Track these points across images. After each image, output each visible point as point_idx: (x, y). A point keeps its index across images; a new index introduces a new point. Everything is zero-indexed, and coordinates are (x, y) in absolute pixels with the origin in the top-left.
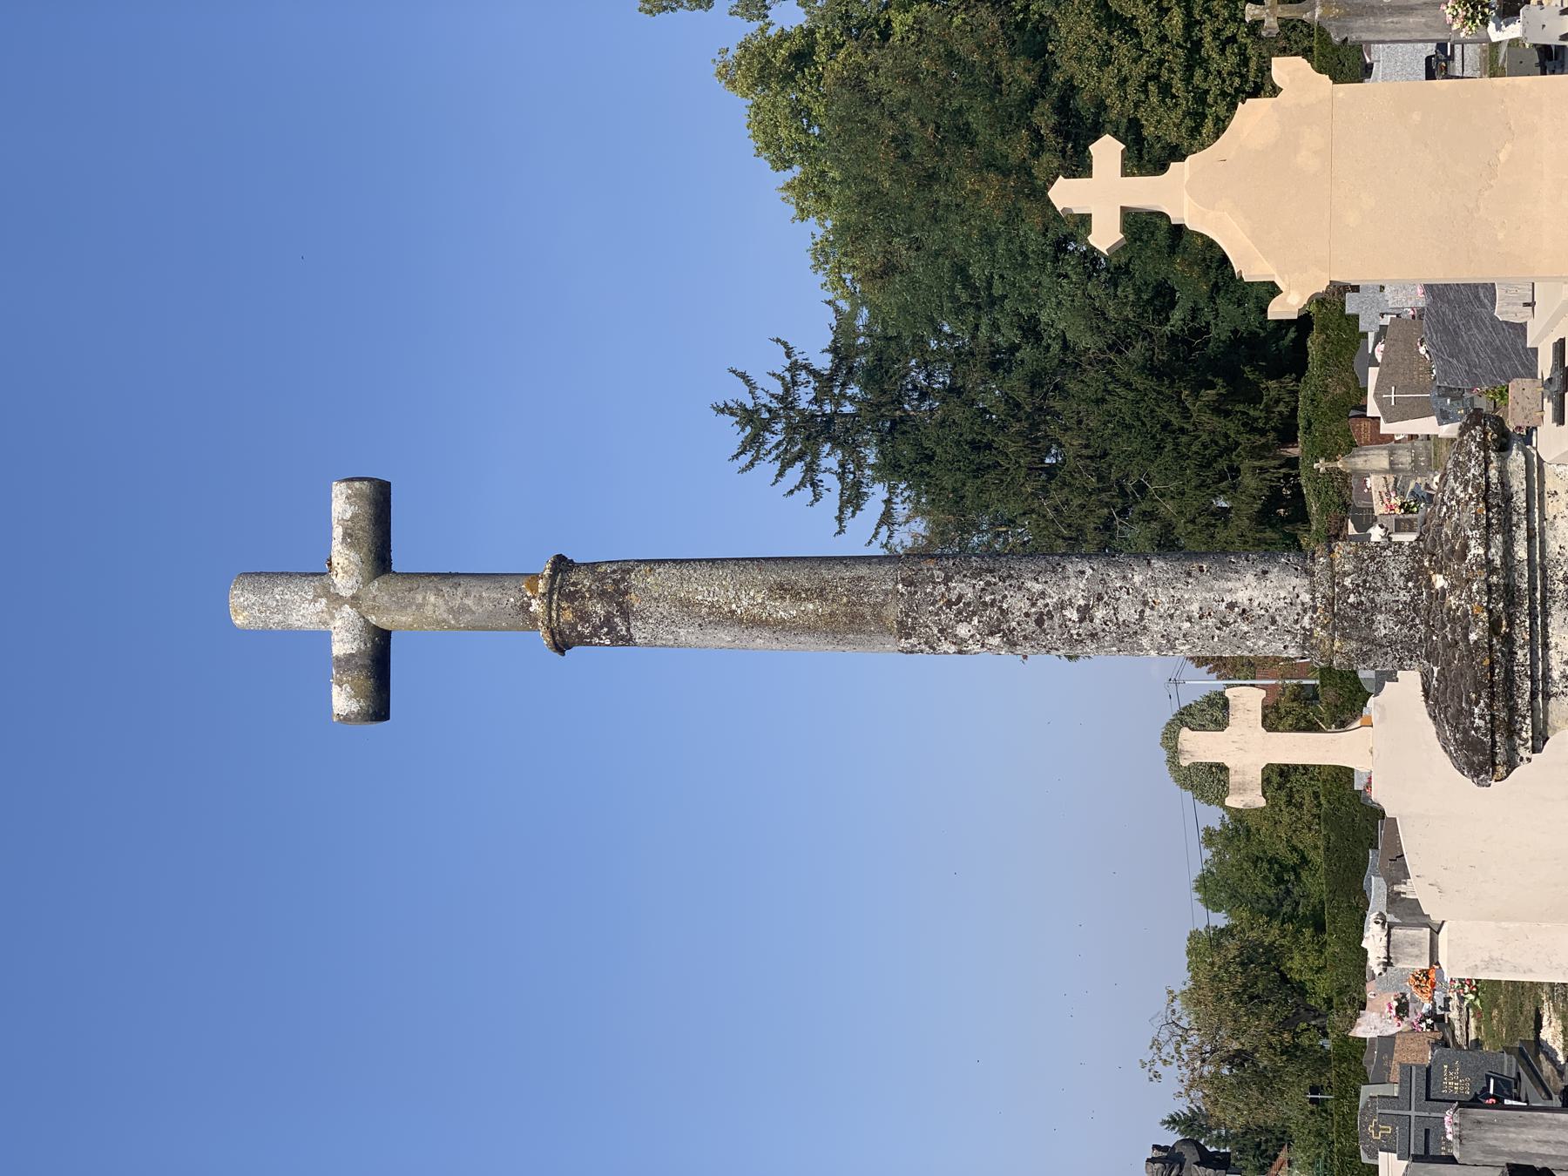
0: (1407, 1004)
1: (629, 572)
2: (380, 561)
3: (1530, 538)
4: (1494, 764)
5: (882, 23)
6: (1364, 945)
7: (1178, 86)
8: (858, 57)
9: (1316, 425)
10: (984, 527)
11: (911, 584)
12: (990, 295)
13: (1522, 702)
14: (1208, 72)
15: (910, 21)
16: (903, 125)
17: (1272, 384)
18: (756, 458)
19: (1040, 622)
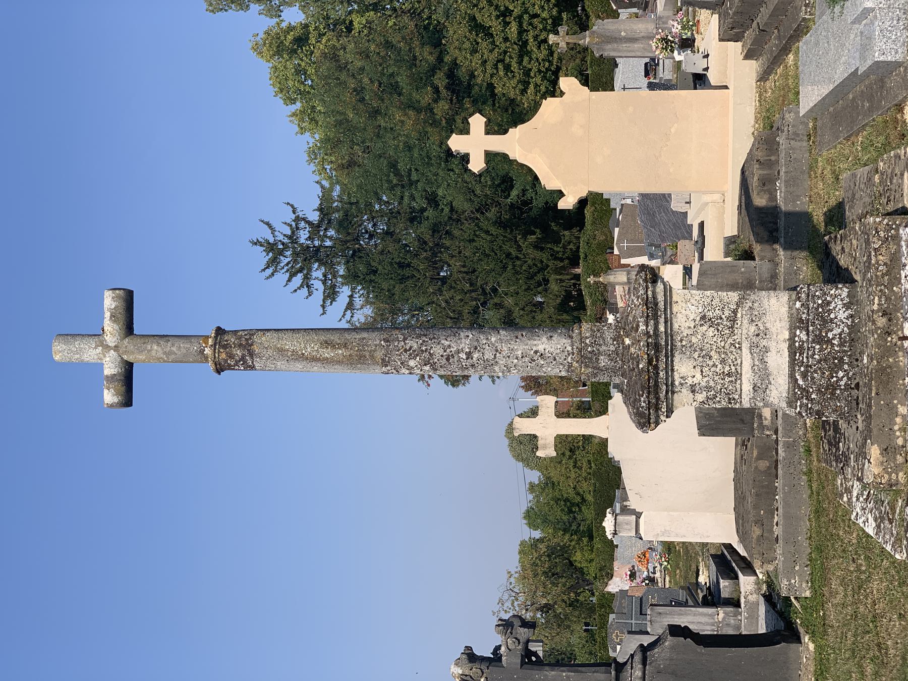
0: (635, 573)
1: (253, 335)
2: (129, 329)
3: (666, 322)
4: (649, 423)
5: (347, 22)
6: (604, 524)
7: (514, 66)
8: (334, 42)
9: (589, 257)
10: (406, 311)
11: (388, 341)
12: (410, 180)
13: (662, 395)
14: (531, 59)
15: (364, 22)
16: (361, 81)
17: (567, 233)
18: (275, 271)
19: (448, 359)
